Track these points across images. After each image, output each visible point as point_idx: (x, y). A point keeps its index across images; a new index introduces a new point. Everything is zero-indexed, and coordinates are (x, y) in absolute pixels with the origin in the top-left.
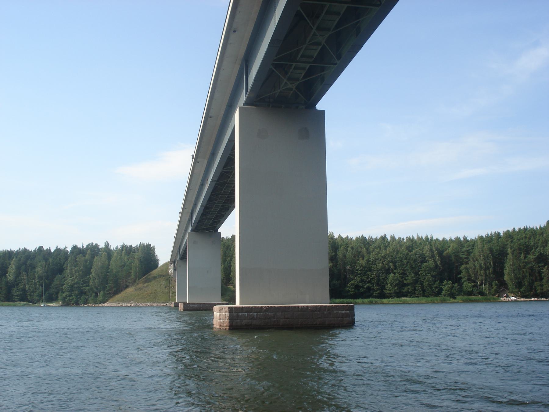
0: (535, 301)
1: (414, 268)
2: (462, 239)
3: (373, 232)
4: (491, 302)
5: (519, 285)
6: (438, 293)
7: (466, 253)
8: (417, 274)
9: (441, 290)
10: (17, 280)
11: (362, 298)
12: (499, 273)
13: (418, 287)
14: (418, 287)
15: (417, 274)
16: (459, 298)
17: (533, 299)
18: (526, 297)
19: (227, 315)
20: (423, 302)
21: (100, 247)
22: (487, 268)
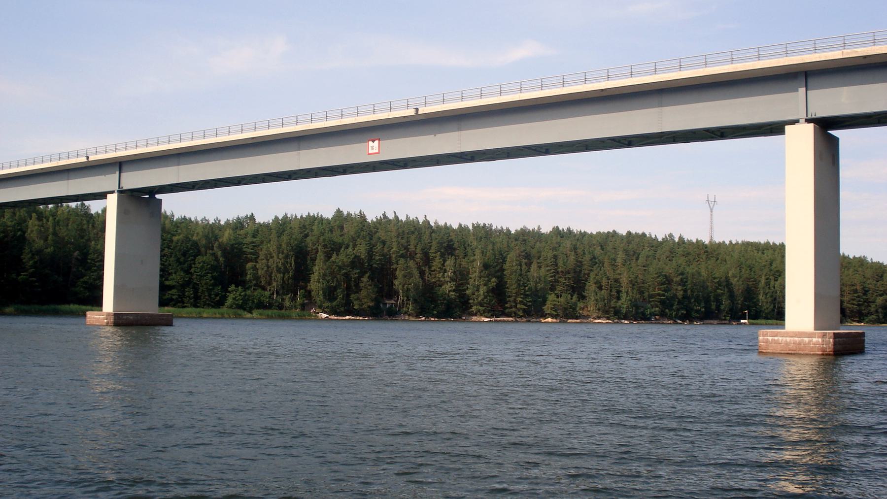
0: (349, 319)
1: (181, 263)
2: (677, 240)
3: (623, 224)
4: (306, 319)
5: (330, 294)
6: (219, 304)
7: (251, 246)
8: (187, 271)
9: (225, 298)
10: (772, 268)
11: (79, 304)
12: (301, 274)
13: (189, 292)
14: (189, 292)
15: (187, 271)
16: (255, 313)
17: (347, 317)
18: (338, 314)
19: (831, 340)
20: (205, 315)
21: (369, 220)
22: (286, 271)
